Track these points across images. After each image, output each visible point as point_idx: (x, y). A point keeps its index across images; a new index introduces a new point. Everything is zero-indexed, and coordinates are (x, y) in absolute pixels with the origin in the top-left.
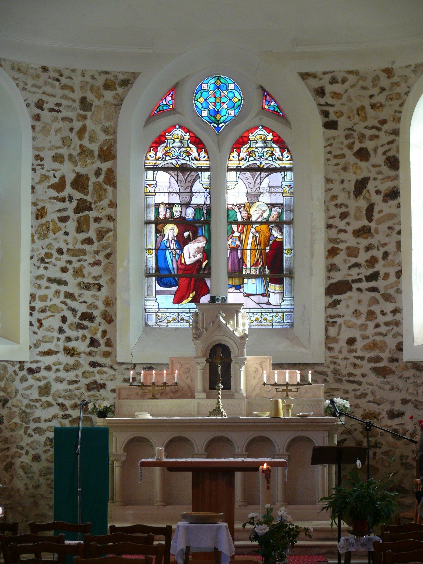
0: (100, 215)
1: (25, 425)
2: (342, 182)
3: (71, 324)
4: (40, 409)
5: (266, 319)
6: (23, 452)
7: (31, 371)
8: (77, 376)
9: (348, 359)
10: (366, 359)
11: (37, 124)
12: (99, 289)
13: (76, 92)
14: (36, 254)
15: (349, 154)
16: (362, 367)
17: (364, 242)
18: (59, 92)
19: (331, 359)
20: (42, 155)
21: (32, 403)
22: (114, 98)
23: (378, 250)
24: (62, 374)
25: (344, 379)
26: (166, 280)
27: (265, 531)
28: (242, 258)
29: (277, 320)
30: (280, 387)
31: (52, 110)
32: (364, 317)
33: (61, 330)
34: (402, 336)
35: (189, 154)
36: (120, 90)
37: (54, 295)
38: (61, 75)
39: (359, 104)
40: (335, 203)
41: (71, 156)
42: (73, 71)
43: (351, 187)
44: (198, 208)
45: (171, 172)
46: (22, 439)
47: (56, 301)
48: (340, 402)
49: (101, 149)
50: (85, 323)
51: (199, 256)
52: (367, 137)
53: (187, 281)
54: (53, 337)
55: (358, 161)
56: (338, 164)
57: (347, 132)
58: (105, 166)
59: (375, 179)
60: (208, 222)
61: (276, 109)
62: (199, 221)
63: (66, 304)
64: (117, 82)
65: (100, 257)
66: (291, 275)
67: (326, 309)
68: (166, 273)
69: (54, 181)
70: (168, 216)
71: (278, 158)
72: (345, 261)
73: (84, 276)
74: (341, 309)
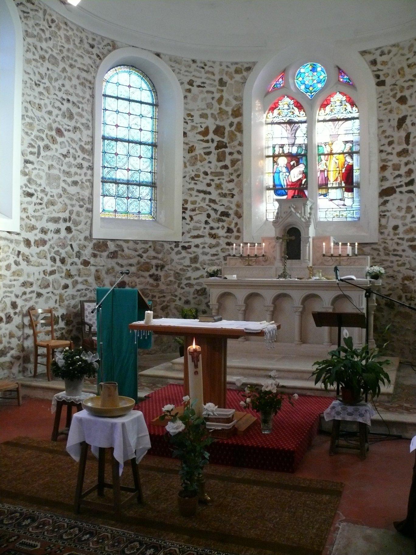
0: (232, 151)
1: (178, 282)
2: (389, 120)
3: (214, 219)
4: (191, 271)
5: (342, 215)
6: (177, 299)
7: (184, 248)
8: (217, 251)
9: (393, 240)
10: (405, 239)
11: (188, 94)
12: (232, 197)
13: (216, 76)
14: (188, 175)
15: (393, 101)
16: (402, 245)
17: (404, 160)
18: (204, 75)
19: (382, 240)
20: (192, 113)
21: (185, 268)
22: (242, 78)
23: (413, 164)
24: (207, 250)
25: (390, 253)
26: (280, 192)
27: (180, 430)
28: (327, 177)
29: (349, 215)
30: (335, 258)
31: (199, 86)
32: (404, 211)
33: (206, 223)
34: (184, 143)
35: (293, 113)
36: (245, 74)
37: (201, 201)
38: (205, 65)
39: (399, 66)
40: (384, 135)
41: (212, 114)
42: (214, 62)
43: (395, 123)
44: (300, 146)
45: (282, 125)
46: (176, 291)
47: (203, 205)
48: (377, 269)
49: (233, 111)
50: (224, 218)
51: (301, 176)
52: (405, 88)
53: (293, 192)
54: (201, 227)
55: (399, 105)
56: (386, 109)
57: (392, 87)
58: (236, 121)
59: (411, 116)
60: (305, 155)
61: (348, 81)
62: (300, 155)
63: (210, 206)
64: (243, 69)
65: (234, 177)
66: (358, 186)
67: (379, 206)
68: (280, 187)
69: (200, 130)
70: (281, 152)
71: (350, 112)
72: (391, 173)
73: (222, 189)
74: (389, 206)
